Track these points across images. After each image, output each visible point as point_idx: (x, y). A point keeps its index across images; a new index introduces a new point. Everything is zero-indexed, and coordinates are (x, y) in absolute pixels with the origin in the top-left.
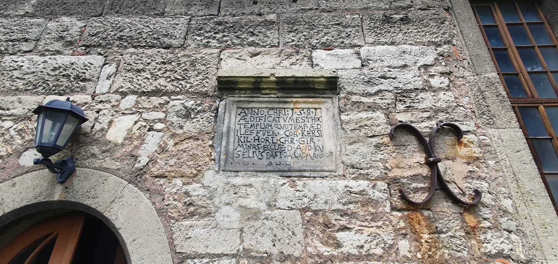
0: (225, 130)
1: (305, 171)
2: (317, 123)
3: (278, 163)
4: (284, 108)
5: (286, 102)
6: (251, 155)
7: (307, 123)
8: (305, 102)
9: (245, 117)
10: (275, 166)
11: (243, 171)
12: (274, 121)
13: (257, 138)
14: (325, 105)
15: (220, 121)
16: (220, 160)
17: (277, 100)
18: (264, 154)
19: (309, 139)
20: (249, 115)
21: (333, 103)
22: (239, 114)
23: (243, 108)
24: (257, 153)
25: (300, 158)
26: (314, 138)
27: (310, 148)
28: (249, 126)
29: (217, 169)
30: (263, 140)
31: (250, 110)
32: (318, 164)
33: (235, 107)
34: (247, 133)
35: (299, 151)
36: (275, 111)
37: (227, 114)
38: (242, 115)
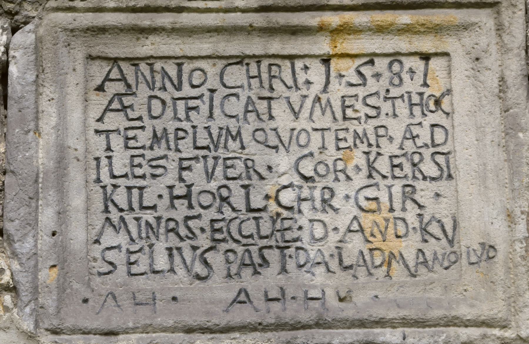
0: (42, 156)
1: (381, 323)
2: (432, 118)
3: (274, 294)
4: (292, 58)
5: (295, 31)
6: (162, 262)
7: (389, 122)
8: (380, 30)
9: (127, 101)
10: (261, 304)
11: (134, 330)
12: (251, 117)
13: (180, 190)
14: (468, 39)
15: (23, 120)
16: (35, 290)
17: (258, 20)
18: (216, 259)
19: (397, 189)
20: (143, 92)
21: (500, 28)
22: (100, 88)
23: (115, 60)
24: (188, 254)
25: (362, 272)
26: (420, 185)
27: (401, 230)
28: (144, 138)
29: (28, 325)
30: (206, 199)
31: (143, 67)
32: (435, 294)
33: (80, 55)
34: (139, 172)
35: (355, 244)
36: (254, 71)
37: (48, 91)
38: (112, 88)
